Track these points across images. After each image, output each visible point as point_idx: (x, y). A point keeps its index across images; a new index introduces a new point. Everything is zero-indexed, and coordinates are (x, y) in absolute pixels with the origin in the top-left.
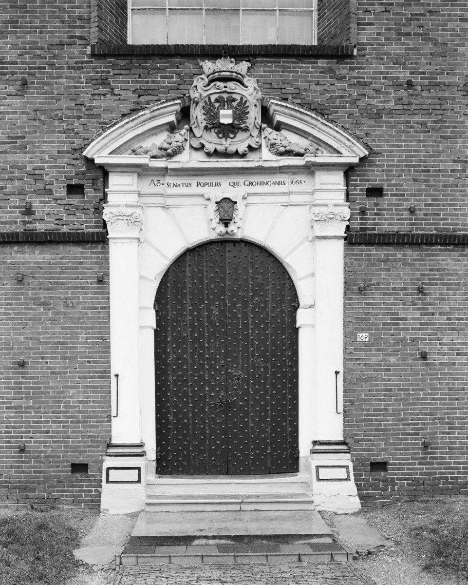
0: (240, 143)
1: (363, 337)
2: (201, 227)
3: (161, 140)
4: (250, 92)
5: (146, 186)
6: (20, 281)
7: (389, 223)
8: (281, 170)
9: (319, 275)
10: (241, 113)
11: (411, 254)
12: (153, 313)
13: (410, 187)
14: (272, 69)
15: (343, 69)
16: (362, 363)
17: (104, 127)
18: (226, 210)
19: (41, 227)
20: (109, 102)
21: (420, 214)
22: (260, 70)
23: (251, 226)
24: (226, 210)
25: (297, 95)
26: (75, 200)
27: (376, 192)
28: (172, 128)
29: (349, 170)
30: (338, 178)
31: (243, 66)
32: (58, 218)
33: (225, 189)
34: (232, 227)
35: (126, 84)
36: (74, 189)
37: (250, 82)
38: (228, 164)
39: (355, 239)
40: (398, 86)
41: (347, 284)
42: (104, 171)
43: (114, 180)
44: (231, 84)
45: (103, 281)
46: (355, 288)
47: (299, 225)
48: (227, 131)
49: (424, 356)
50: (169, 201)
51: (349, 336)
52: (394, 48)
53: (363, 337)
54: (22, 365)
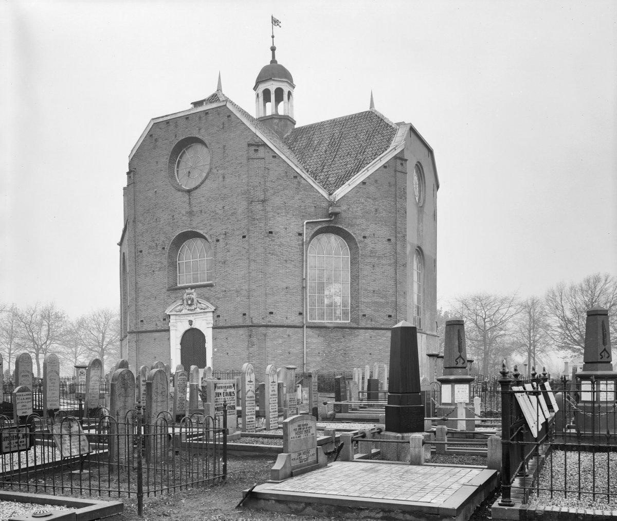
0: (193, 307)
1: (216, 350)
2: (188, 327)
3: (179, 308)
4: (194, 296)
5: (178, 317)
6: (155, 340)
7: (221, 324)
8: (201, 313)
9: (208, 334)
10: (192, 301)
11: (225, 330)
12: (180, 351)
13: (225, 315)
14: (199, 290)
15: (212, 289)
16: (301, 414)
17: (169, 305)
18: (191, 322)
19: (159, 328)
20: (170, 300)
21: (227, 321)
22: (197, 291)
23: (196, 325)
24: (191, 322)
25: (203, 295)
26: (164, 322)
27: (218, 316)
28: (181, 305)
29: (213, 312)
30: (211, 314)
31: (193, 290)
32: (434, 353)
33: (191, 318)
34: (192, 326)
35: (173, 296)
36: (164, 320)
37: (195, 294)
38: (193, 312)
39: (214, 328)
40: (222, 291)
41: (213, 337)
42: (169, 316)
43: (171, 317)
44: (190, 295)
45: (169, 339)
46: (214, 339)
47: (204, 324)
48: (190, 305)
49: (228, 354)
50: (182, 321)
51: (213, 349)
52: (222, 283)
53: (216, 350)
54: (155, 357)
